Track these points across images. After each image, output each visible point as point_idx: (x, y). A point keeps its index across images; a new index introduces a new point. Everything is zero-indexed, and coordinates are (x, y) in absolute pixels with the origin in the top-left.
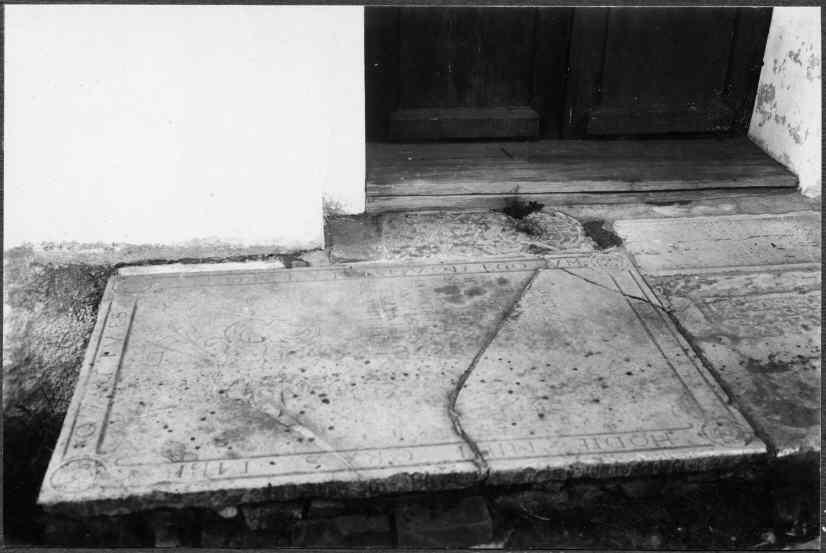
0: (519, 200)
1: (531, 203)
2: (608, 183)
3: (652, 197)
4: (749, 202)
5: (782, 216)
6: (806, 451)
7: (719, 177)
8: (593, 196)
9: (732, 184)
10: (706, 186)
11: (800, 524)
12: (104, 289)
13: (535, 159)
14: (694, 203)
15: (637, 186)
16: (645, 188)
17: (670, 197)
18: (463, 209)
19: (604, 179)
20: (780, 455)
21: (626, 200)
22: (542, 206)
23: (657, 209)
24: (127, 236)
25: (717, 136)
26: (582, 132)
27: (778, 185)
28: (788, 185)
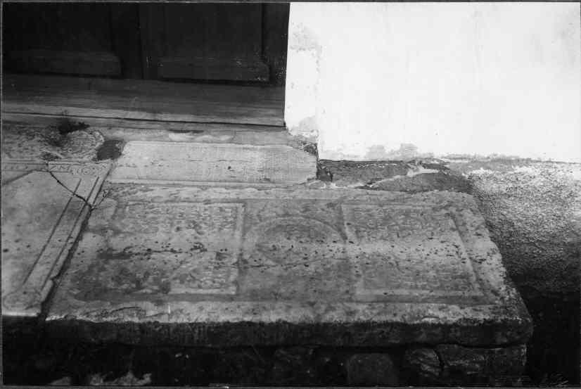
0: (70, 121)
1: (80, 123)
2: (136, 113)
3: (173, 126)
4: (250, 134)
5: (259, 147)
6: (69, 318)
7: (221, 115)
8: (129, 122)
9: (233, 121)
10: (213, 120)
11: (420, 361)
12: (316, 148)
13: (103, 92)
14: (205, 132)
15: (159, 117)
16: (165, 119)
17: (186, 127)
18: (27, 124)
19: (143, 110)
20: (48, 319)
21: (153, 126)
22: (88, 126)
23: (173, 136)
24: (289, 108)
25: (262, 85)
26: (154, 75)
27: (269, 124)
28: (276, 124)
